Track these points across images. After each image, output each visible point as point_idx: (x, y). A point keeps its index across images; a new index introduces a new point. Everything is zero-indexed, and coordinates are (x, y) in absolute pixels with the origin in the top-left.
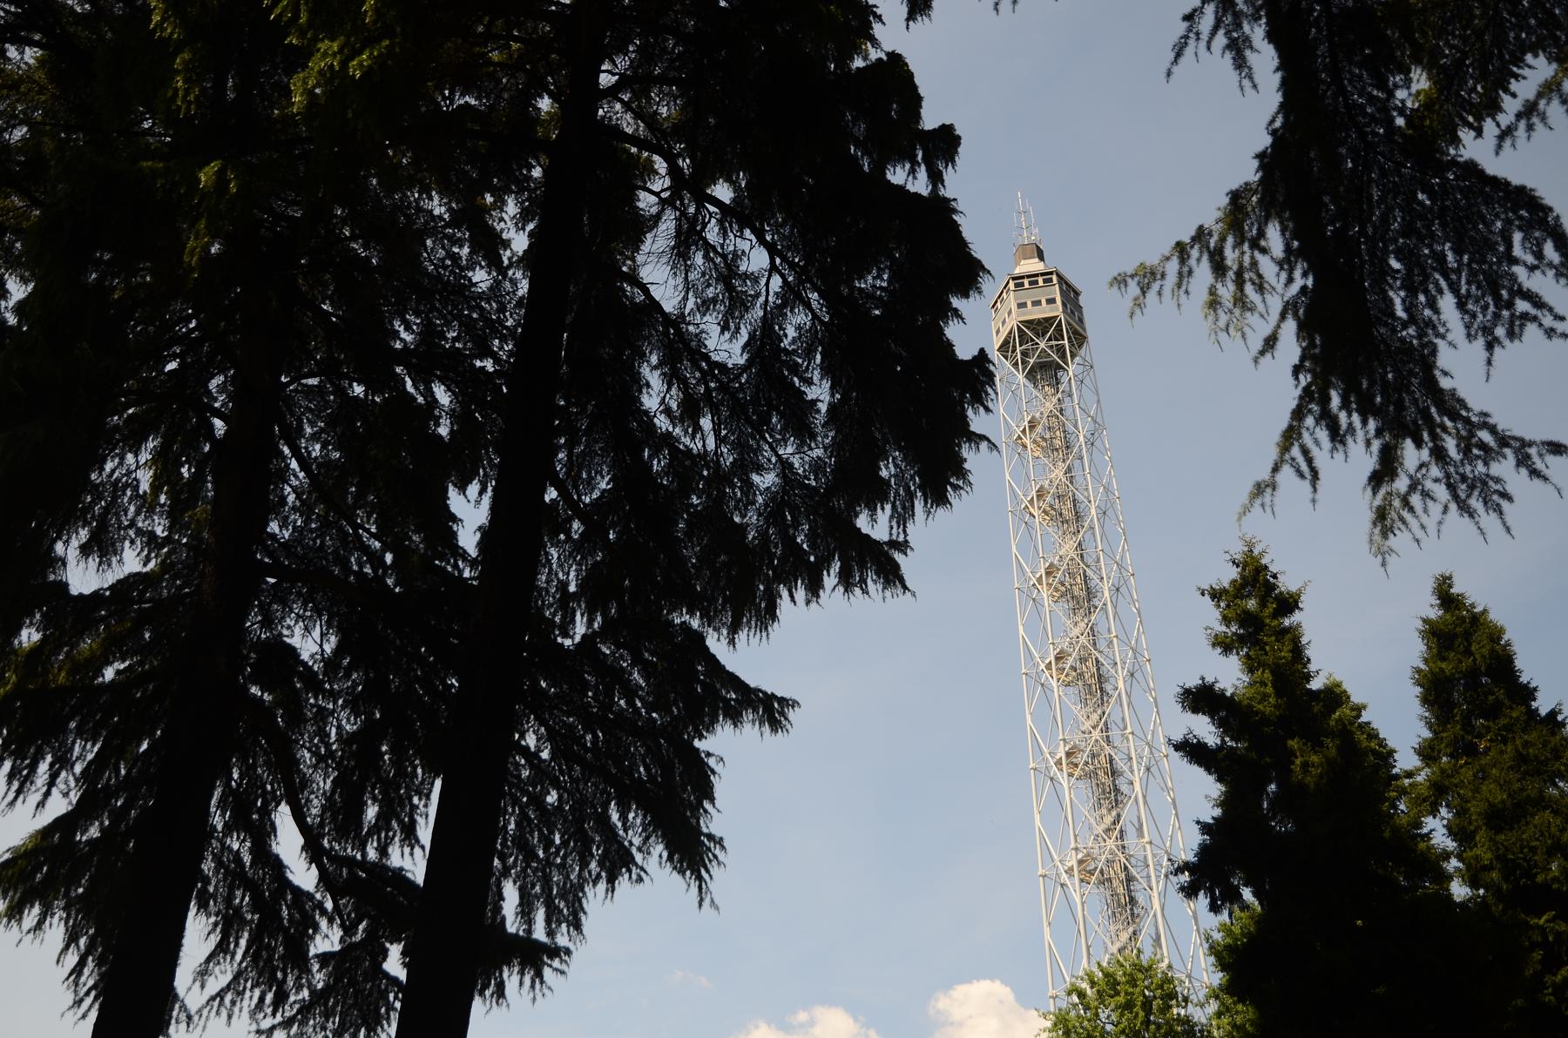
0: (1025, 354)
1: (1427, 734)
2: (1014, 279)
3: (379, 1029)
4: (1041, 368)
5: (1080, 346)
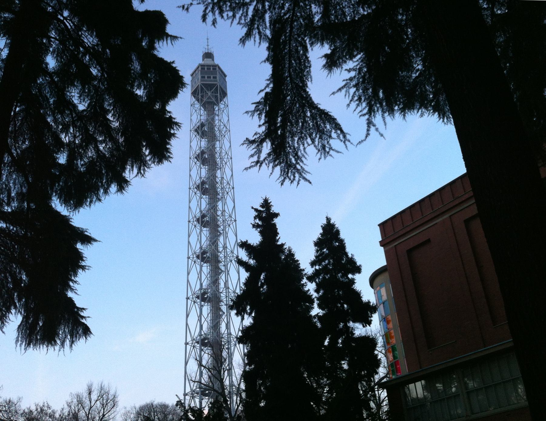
0: (202, 96)
1: (244, 35)
2: (201, 66)
3: (71, 284)
4: (208, 103)
5: (224, 97)
